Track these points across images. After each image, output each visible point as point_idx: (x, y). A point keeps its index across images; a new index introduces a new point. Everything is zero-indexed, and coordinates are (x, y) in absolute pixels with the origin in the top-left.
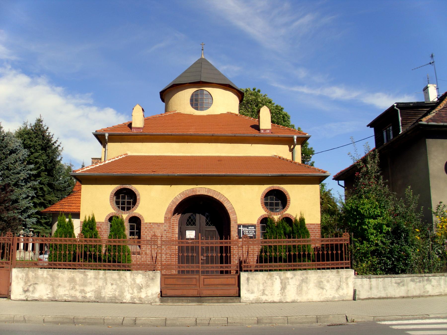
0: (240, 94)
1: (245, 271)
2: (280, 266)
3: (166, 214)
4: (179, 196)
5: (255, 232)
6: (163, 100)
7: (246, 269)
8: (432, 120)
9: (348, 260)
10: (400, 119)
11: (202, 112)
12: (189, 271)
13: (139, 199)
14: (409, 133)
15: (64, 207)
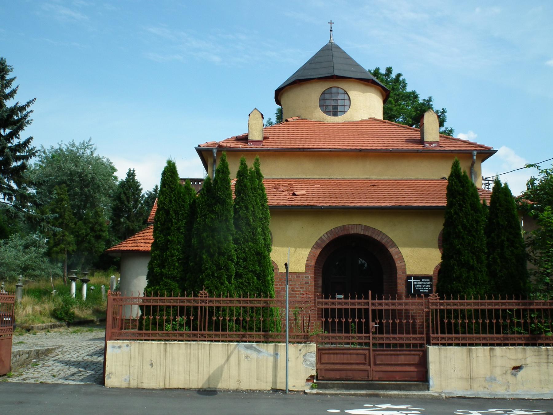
4: (326, 235)
5: (431, 286)
6: (278, 102)
7: (435, 342)
12: (410, 344)
15: (139, 244)
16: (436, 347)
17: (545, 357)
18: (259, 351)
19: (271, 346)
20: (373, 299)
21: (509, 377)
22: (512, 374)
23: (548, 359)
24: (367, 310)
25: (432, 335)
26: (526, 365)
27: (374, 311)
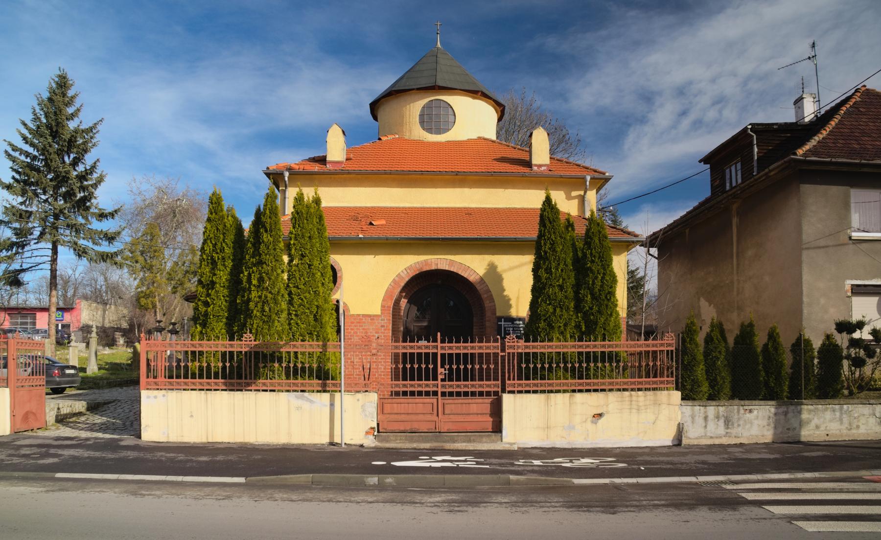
0: (500, 108)
1: (509, 392)
2: (535, 385)
3: (384, 300)
8: (813, 152)
9: (496, 379)
10: (756, 150)
11: (439, 136)
13: (341, 277)
14: (772, 173)
16: (511, 395)
19: (326, 396)
20: (443, 341)
21: (589, 424)
22: (592, 422)
24: (435, 355)
25: (507, 382)
26: (608, 412)
27: (443, 355)
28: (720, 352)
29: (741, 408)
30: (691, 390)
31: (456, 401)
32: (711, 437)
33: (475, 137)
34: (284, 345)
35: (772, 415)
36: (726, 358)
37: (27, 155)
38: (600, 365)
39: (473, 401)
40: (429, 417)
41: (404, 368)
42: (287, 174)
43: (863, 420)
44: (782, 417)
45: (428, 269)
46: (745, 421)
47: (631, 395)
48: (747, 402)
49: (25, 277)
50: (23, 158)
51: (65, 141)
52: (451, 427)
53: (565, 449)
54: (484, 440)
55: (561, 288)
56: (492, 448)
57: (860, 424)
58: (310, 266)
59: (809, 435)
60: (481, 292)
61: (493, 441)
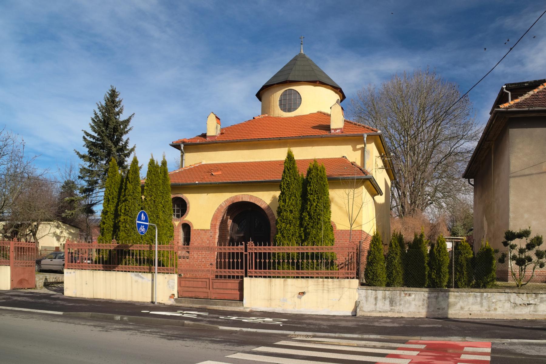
1: (250, 277)
3: (212, 221)
9: (242, 268)
13: (189, 207)
17: (321, 286)
18: (142, 278)
21: (296, 299)
22: (298, 297)
23: (323, 287)
25: (248, 270)
26: (308, 292)
28: (396, 254)
29: (402, 292)
30: (373, 279)
31: (220, 281)
32: (380, 312)
33: (316, 112)
34: (131, 246)
35: (426, 298)
36: (401, 258)
37: (94, 137)
38: (310, 261)
39: (229, 281)
40: (205, 290)
41: (229, 262)
42: (182, 146)
43: (500, 304)
44: (434, 300)
45: (237, 201)
46: (405, 301)
47: (323, 281)
48: (406, 289)
49: (94, 208)
50: (92, 140)
51: (111, 128)
52: (216, 296)
53: (281, 314)
54: (233, 305)
55: (291, 211)
56: (233, 310)
57: (497, 307)
58: (154, 201)
59: (455, 314)
60: (268, 215)
61: (238, 306)
